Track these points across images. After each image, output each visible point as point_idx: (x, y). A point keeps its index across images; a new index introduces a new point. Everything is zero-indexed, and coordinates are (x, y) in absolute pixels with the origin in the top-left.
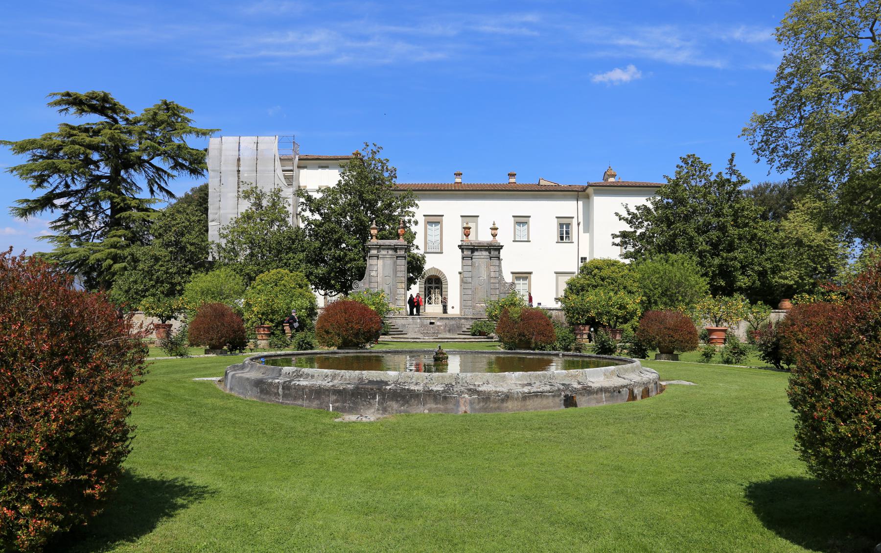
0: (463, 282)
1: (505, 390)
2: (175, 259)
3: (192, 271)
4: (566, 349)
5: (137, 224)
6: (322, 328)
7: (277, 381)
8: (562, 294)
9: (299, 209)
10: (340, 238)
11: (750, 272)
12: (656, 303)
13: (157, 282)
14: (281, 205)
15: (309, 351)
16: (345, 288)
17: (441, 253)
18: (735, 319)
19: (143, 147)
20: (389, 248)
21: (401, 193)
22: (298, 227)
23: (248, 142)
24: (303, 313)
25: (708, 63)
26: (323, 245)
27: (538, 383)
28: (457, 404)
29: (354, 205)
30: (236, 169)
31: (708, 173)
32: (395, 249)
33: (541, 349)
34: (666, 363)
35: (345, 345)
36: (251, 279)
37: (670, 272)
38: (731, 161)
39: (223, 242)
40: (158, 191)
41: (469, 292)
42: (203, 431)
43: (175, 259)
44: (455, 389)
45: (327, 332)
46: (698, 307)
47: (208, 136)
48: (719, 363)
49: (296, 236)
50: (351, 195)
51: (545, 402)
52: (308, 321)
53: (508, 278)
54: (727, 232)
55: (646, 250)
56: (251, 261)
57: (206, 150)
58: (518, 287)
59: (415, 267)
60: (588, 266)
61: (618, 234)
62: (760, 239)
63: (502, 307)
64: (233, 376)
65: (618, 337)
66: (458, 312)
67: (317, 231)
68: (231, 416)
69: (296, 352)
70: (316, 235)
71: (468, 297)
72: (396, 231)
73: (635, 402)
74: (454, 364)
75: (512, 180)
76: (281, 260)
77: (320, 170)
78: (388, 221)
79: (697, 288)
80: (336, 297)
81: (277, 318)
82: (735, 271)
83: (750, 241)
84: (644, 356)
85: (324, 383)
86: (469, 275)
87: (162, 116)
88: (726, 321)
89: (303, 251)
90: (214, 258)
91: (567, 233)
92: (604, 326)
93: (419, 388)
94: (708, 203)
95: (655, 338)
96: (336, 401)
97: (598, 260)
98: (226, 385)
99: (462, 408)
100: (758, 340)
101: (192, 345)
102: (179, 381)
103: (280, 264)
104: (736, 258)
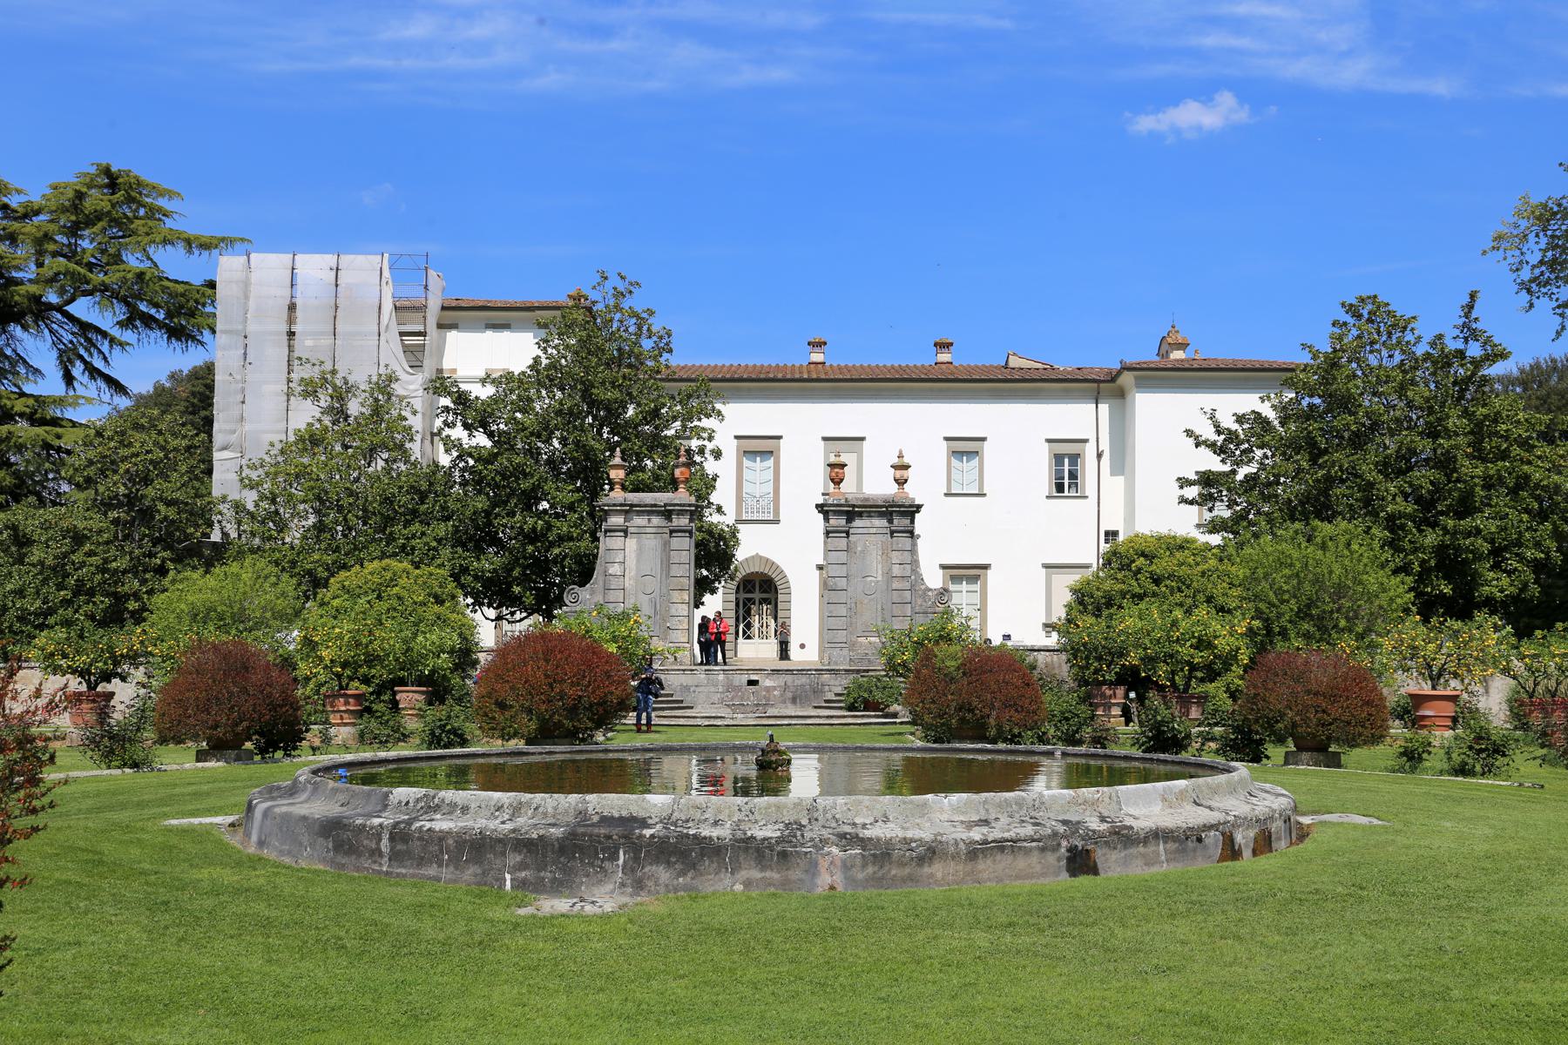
0: (827, 587)
1: (926, 835)
2: (126, 537)
3: (170, 565)
4: (1071, 740)
5: (28, 455)
6: (489, 695)
7: (376, 821)
8: (1059, 613)
9: (438, 423)
10: (535, 488)
11: (1513, 563)
12: (1284, 633)
13: (76, 593)
14: (395, 413)
15: (458, 750)
16: (547, 603)
17: (777, 522)
18: (1477, 670)
19: (47, 272)
20: (652, 510)
21: (683, 386)
22: (436, 464)
23: (314, 267)
24: (444, 661)
25: (1417, 85)
26: (494, 505)
27: (1004, 820)
28: (812, 868)
29: (571, 413)
30: (285, 328)
31: (1409, 337)
32: (667, 514)
33: (1011, 741)
34: (1309, 773)
35: (545, 734)
36: (318, 583)
37: (1318, 563)
38: (1470, 307)
39: (250, 498)
40: (85, 379)
41: (842, 610)
42: (186, 947)
43: (126, 537)
44: (808, 835)
45: (502, 706)
46: (1387, 643)
47: (215, 252)
48: (1441, 773)
49: (429, 485)
50: (562, 389)
51: (1021, 863)
52: (456, 680)
53: (933, 579)
54: (1455, 470)
55: (1258, 513)
56: (319, 541)
57: (212, 285)
58: (955, 599)
59: (714, 554)
60: (1122, 550)
61: (1193, 477)
62: (1537, 486)
63: (919, 643)
64: (266, 813)
65: (1195, 713)
66: (815, 658)
67: (481, 473)
68: (260, 908)
69: (424, 752)
70: (479, 482)
71: (840, 623)
72: (669, 470)
73: (1237, 864)
74: (805, 776)
75: (944, 357)
76: (391, 539)
77: (489, 333)
78: (651, 449)
79: (1383, 600)
80: (524, 624)
81: (379, 673)
82: (1474, 560)
83: (1514, 492)
84: (1256, 758)
85: (493, 824)
86: (842, 571)
87: (97, 200)
88: (1456, 675)
89: (448, 518)
90: (225, 535)
91: (1073, 475)
92: (1161, 688)
93: (723, 832)
94: (1410, 405)
95: (1282, 715)
96: (522, 866)
97: (1144, 537)
98: (248, 835)
99: (824, 879)
100: (1536, 719)
101: (163, 740)
102: (127, 828)
103: (390, 549)
104: (1478, 531)
